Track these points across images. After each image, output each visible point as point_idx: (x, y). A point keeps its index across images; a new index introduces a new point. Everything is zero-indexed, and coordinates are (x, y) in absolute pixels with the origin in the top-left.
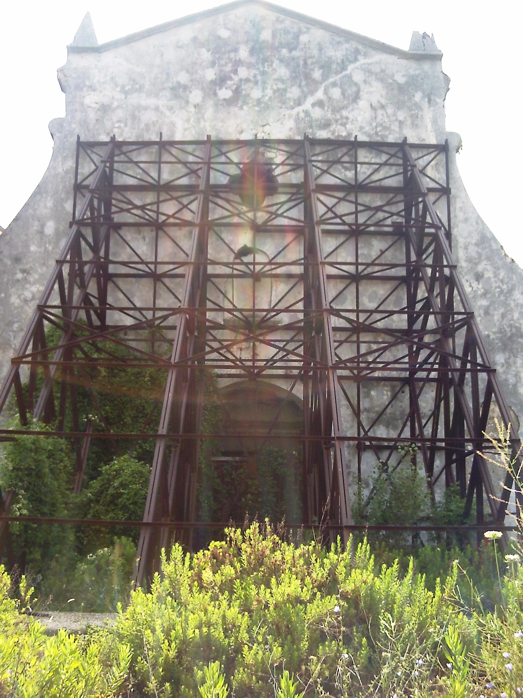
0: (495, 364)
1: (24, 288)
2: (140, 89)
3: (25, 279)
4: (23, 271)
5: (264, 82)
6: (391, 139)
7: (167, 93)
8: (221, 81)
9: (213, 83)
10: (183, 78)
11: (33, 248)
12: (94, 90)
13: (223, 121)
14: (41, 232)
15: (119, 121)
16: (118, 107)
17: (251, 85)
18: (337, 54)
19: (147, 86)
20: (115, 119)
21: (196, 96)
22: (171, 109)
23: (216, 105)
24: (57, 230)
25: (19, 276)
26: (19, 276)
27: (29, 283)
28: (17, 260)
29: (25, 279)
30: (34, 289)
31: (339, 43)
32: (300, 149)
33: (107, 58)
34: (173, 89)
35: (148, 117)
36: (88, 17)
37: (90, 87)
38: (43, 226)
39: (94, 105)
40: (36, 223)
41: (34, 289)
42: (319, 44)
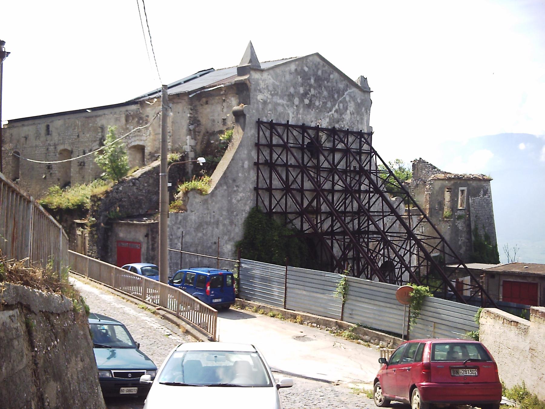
0: (131, 154)
1: (237, 195)
2: (277, 94)
3: (237, 190)
4: (237, 186)
5: (320, 98)
6: (355, 130)
7: (286, 98)
8: (305, 94)
9: (302, 94)
10: (292, 90)
11: (240, 175)
12: (261, 92)
13: (306, 115)
14: (243, 167)
15: (270, 110)
16: (270, 103)
17: (315, 98)
18: (341, 86)
19: (280, 93)
20: (268, 109)
21: (296, 101)
22: (288, 106)
23: (304, 107)
24: (249, 166)
25: (235, 189)
26: (235, 189)
27: (239, 192)
28: (234, 181)
29: (237, 190)
30: (241, 195)
31: (342, 80)
32: (332, 132)
33: (265, 75)
34: (289, 96)
35: (280, 109)
36: (251, 46)
37: (259, 90)
38: (243, 163)
39: (261, 101)
40: (241, 162)
41: (241, 195)
42: (336, 80)
